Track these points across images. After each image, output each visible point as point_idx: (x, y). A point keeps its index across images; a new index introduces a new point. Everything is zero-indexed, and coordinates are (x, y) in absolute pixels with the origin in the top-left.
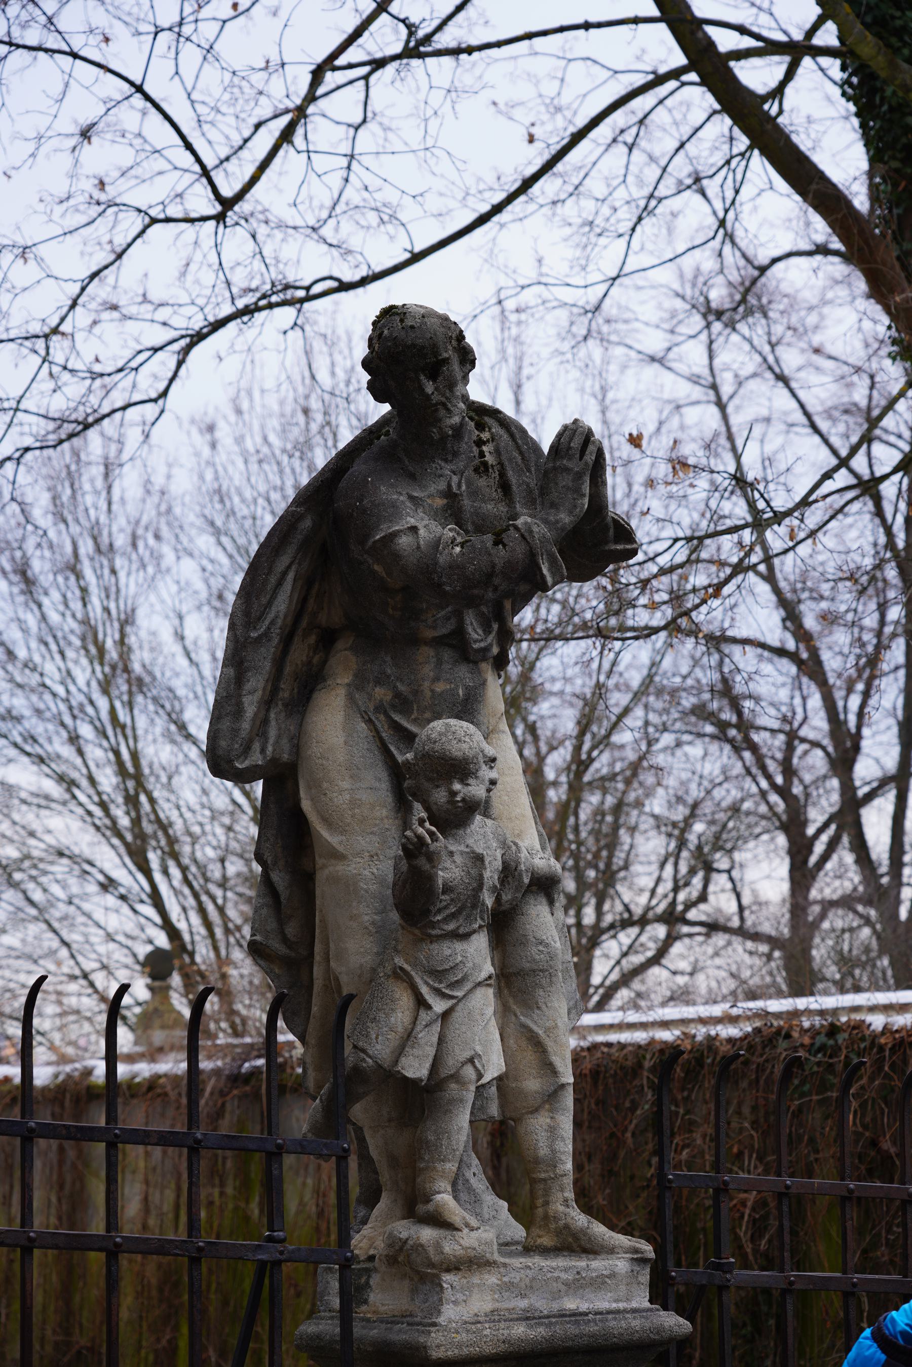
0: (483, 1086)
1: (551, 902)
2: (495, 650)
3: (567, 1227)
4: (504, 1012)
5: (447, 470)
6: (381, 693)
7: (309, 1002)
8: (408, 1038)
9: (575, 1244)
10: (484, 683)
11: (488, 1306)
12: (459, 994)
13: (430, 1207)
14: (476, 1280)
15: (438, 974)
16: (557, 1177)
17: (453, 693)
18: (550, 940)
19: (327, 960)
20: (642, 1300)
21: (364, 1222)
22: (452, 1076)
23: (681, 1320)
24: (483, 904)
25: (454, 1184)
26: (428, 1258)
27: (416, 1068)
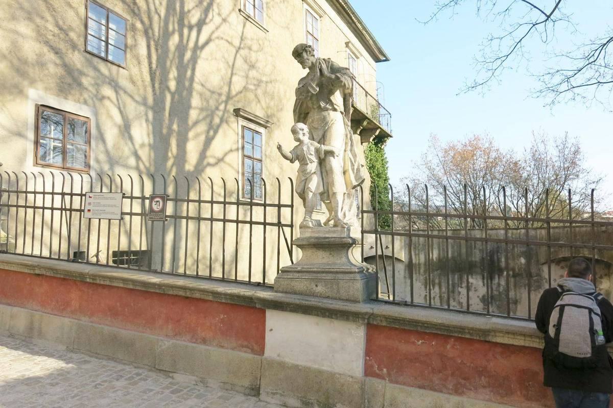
17: (321, 118)
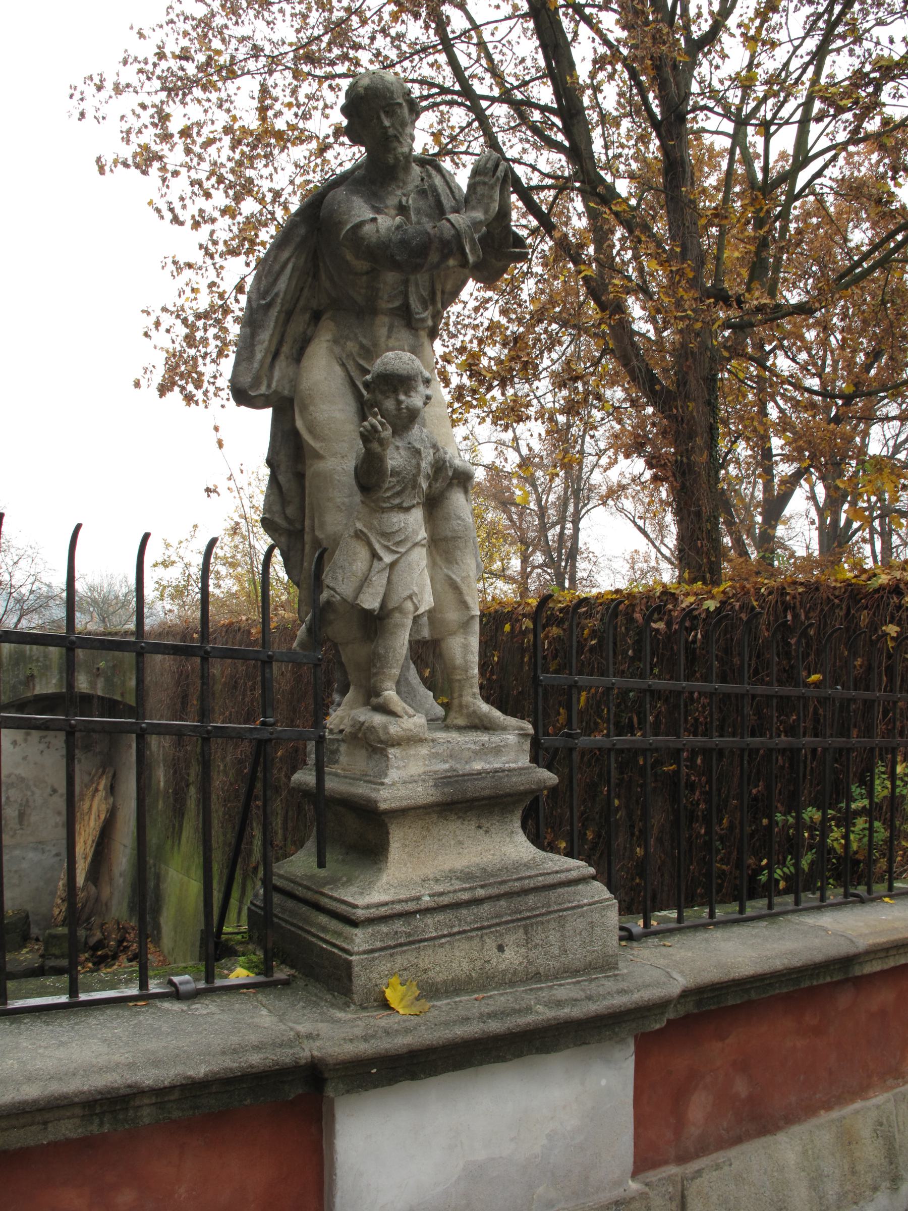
0: (419, 616)
1: (466, 492)
2: (430, 323)
3: (474, 712)
4: (433, 565)
5: (399, 192)
6: (351, 346)
7: (302, 560)
8: (365, 580)
9: (481, 725)
10: (422, 345)
11: (421, 770)
12: (402, 550)
13: (380, 700)
14: (412, 752)
15: (385, 535)
16: (468, 678)
18: (465, 517)
19: (313, 530)
20: (524, 760)
21: (339, 705)
22: (396, 608)
23: (551, 774)
24: (420, 487)
25: (398, 683)
26: (379, 737)
27: (371, 602)
